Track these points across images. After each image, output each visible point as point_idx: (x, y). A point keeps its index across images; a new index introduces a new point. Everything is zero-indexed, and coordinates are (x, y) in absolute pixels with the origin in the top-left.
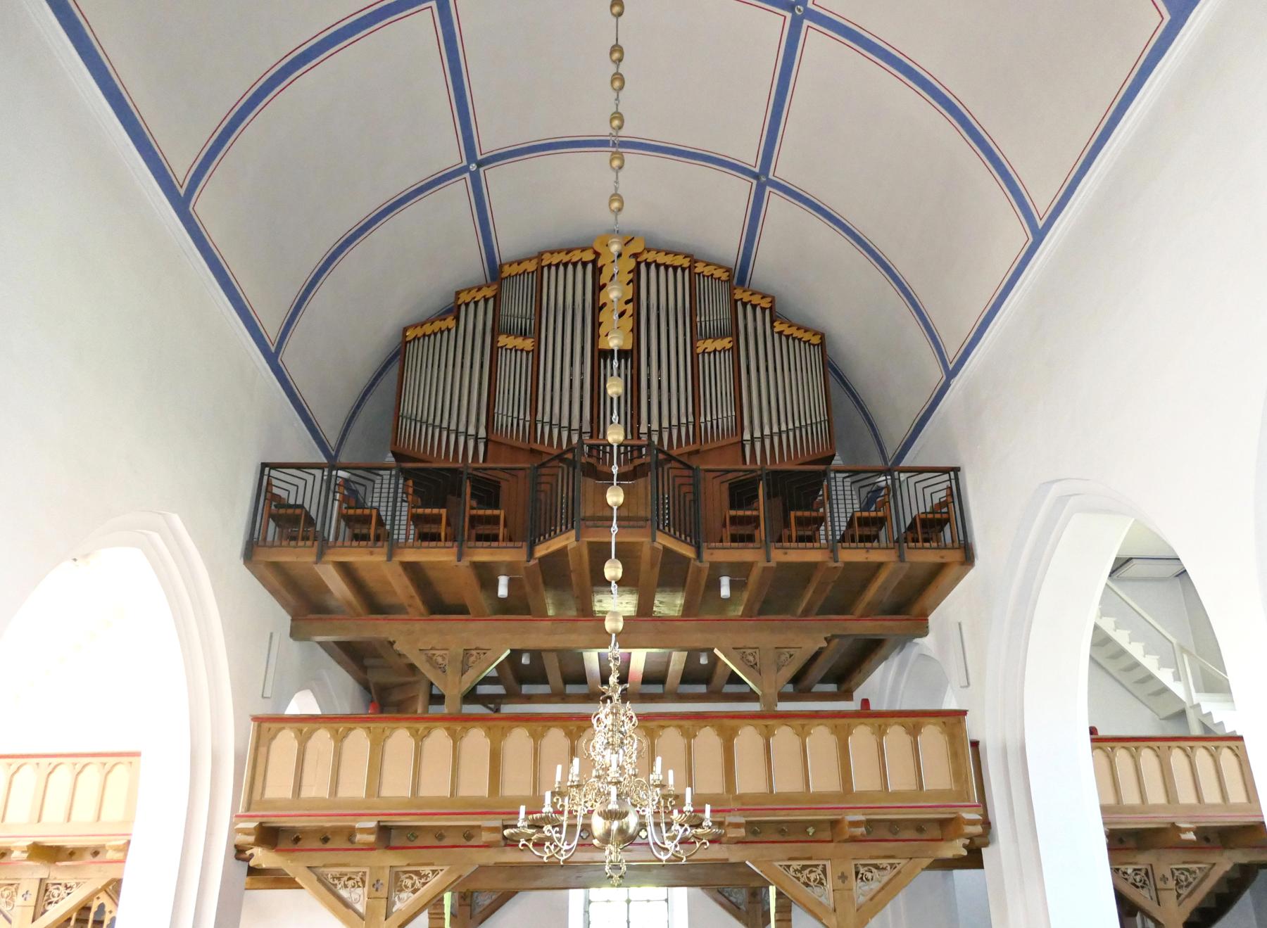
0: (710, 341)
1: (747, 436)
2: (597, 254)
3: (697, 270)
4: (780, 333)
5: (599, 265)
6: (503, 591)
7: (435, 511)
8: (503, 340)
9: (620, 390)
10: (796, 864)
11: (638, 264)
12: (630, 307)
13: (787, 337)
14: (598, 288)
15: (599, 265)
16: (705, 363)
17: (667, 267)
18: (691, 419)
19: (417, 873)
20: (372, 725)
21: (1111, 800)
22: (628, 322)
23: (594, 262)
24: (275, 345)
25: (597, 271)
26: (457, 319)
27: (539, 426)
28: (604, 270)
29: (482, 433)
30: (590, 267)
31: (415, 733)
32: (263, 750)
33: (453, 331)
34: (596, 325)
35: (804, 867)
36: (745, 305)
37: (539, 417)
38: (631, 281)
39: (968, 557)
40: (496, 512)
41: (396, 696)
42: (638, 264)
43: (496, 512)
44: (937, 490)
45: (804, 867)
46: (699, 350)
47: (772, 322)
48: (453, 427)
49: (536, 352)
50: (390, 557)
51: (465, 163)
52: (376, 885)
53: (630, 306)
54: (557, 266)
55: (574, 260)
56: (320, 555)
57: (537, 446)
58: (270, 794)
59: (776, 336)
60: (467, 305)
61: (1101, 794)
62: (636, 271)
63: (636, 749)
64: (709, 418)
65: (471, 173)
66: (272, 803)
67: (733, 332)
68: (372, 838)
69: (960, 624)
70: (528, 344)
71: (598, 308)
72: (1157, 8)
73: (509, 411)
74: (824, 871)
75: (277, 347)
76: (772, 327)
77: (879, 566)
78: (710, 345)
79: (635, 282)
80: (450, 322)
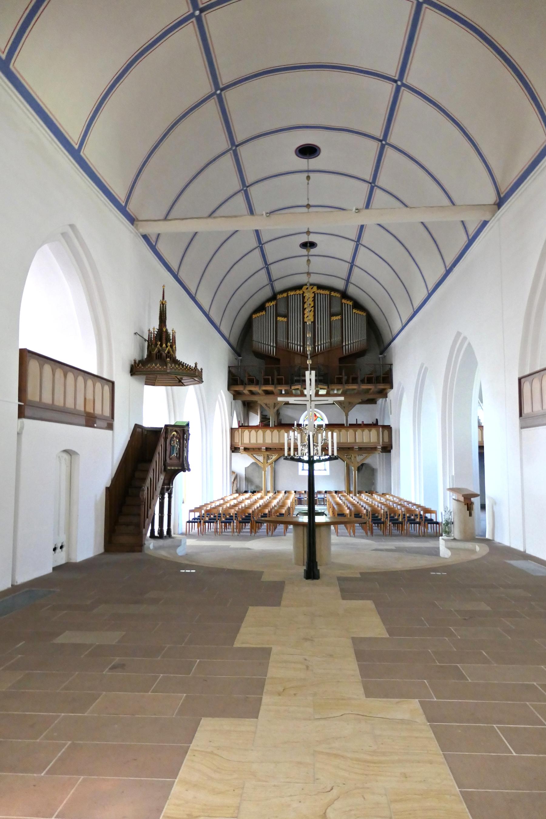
0: (335, 317)
1: (344, 344)
2: (304, 292)
3: (332, 295)
4: (355, 313)
5: (304, 296)
6: (283, 392)
7: (269, 377)
8: (279, 318)
9: (310, 335)
10: (346, 455)
11: (315, 294)
12: (313, 308)
13: (357, 314)
14: (304, 303)
15: (304, 296)
16: (333, 324)
17: (323, 294)
18: (329, 341)
19: (272, 455)
20: (263, 429)
21: (481, 440)
22: (312, 313)
23: (303, 294)
24: (78, 145)
25: (304, 297)
26: (266, 311)
27: (289, 344)
28: (305, 297)
29: (275, 345)
30: (301, 296)
31: (271, 431)
32: (242, 434)
33: (265, 315)
34: (304, 314)
35: (347, 455)
36: (345, 304)
37: (289, 341)
38: (313, 300)
39: (392, 387)
40: (282, 377)
41: (252, 405)
42: (315, 294)
43: (282, 377)
44: (387, 368)
45: (347, 455)
46: (332, 320)
47: (352, 309)
48: (267, 343)
49: (288, 322)
50: (260, 388)
51: (264, 266)
52: (264, 458)
53: (313, 308)
54: (292, 295)
55: (297, 293)
56: (245, 388)
57: (289, 350)
58: (245, 442)
59: (354, 313)
60: (268, 307)
61: (479, 439)
62: (314, 297)
63: (286, 497)
64: (334, 340)
65: (271, 284)
66: (246, 444)
67: (341, 314)
68: (265, 450)
69: (391, 400)
70: (285, 320)
71: (304, 309)
72: (421, 273)
73: (282, 339)
74: (351, 456)
75: (126, 203)
76: (353, 311)
77: (370, 389)
78: (334, 318)
79: (314, 301)
80: (264, 313)
